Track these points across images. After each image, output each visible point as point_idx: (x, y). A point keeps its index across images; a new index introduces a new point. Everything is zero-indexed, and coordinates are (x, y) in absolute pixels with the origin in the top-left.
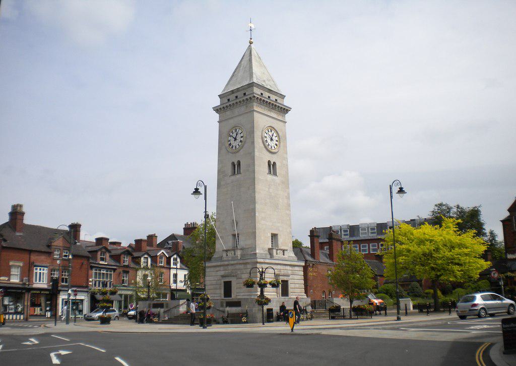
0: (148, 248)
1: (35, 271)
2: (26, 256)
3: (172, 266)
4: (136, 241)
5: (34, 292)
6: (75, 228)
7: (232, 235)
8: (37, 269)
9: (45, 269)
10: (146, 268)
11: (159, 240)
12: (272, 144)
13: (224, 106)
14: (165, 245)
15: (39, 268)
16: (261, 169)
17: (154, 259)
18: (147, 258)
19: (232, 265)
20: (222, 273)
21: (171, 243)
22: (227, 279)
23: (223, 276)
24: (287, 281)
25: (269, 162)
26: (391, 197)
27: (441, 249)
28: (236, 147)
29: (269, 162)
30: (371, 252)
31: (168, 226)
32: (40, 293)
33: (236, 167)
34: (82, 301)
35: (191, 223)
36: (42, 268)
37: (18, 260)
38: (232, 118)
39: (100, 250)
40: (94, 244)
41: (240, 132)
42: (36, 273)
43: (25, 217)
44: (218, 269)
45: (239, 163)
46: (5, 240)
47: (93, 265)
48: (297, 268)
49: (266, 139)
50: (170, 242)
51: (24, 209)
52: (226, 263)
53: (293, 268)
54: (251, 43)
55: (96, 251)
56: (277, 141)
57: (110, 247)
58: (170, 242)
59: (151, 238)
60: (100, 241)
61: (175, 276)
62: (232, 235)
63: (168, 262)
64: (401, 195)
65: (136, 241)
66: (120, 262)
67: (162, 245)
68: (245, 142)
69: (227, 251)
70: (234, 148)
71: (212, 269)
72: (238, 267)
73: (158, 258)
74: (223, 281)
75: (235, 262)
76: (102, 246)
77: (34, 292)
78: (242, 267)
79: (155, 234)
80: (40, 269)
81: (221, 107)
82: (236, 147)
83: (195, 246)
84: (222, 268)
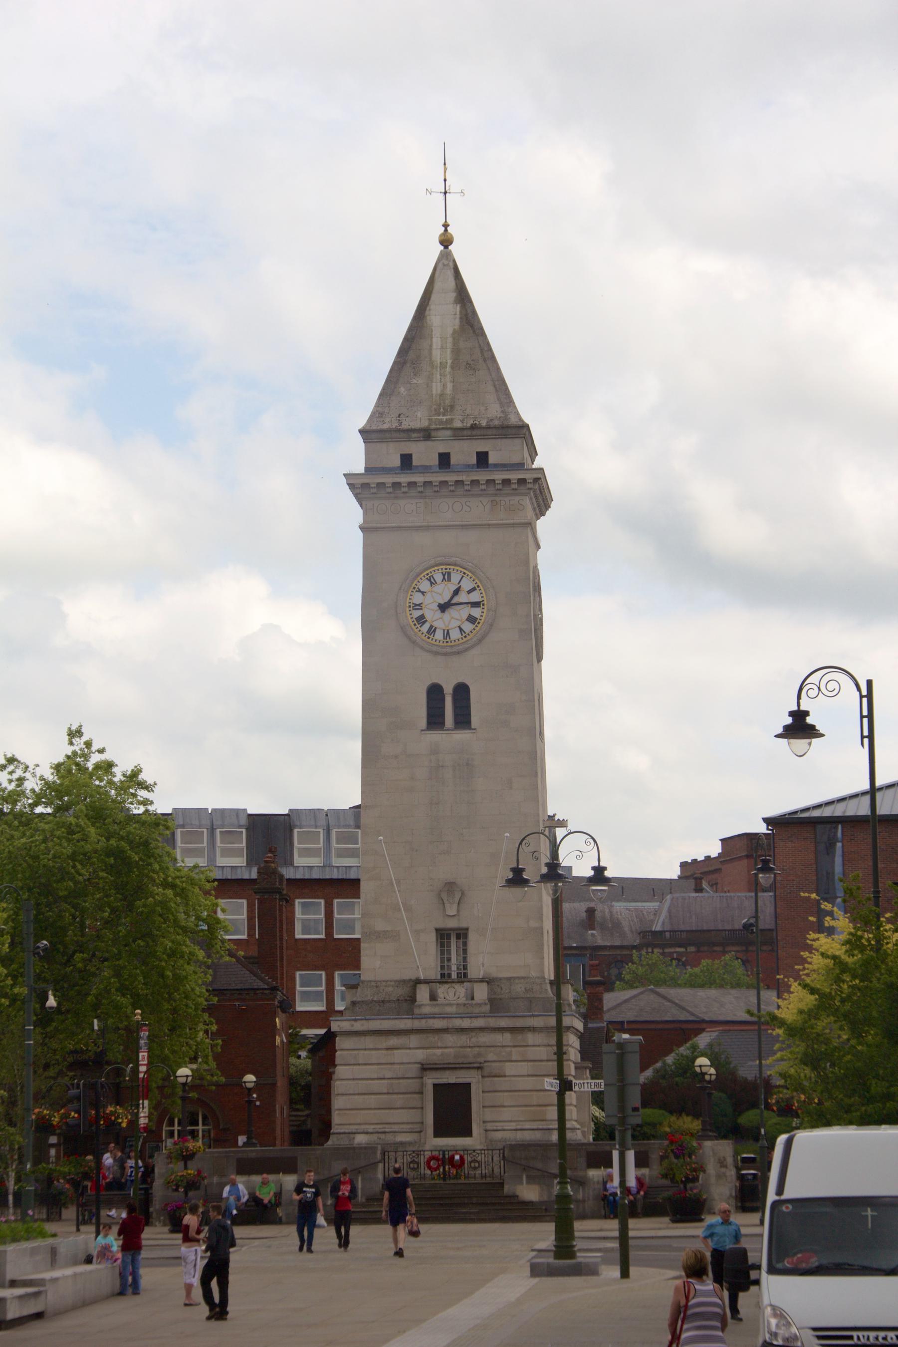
7: (437, 930)
19: (462, 1030)
20: (421, 1055)
23: (426, 1068)
27: (115, 809)
30: (299, 936)
33: (449, 707)
38: (428, 528)
41: (467, 585)
44: (393, 1041)
48: (531, 1038)
53: (520, 1037)
62: (437, 930)
64: (800, 744)
70: (439, 635)
74: (430, 1080)
82: (447, 634)
84: (414, 1040)
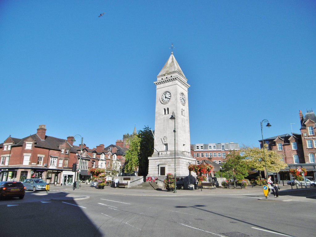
1: (51, 160)
5: (50, 171)
8: (52, 159)
9: (56, 159)
11: (105, 147)
15: (53, 158)
26: (262, 128)
32: (53, 172)
34: (41, 158)
36: (55, 158)
42: (51, 161)
43: (47, 132)
44: (156, 160)
45: (168, 109)
50: (110, 148)
52: (161, 158)
58: (110, 148)
72: (168, 160)
75: (167, 157)
77: (50, 171)
78: (206, 161)
80: (54, 159)
82: (164, 101)
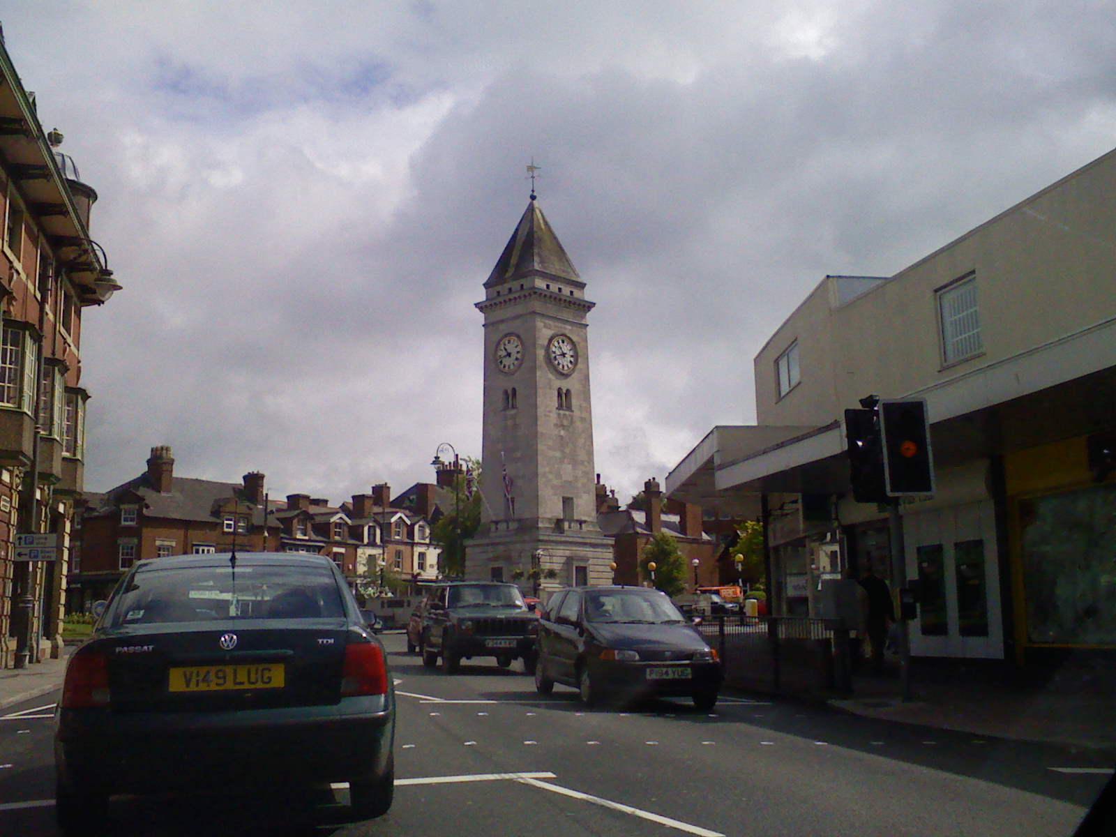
0: (377, 509)
2: (180, 533)
3: (417, 540)
4: (354, 497)
6: (254, 481)
10: (372, 544)
12: (566, 362)
13: (493, 302)
14: (403, 502)
16: (547, 402)
17: (386, 528)
18: (374, 527)
21: (417, 498)
22: (496, 565)
23: (490, 560)
24: (585, 568)
25: (560, 390)
28: (509, 367)
29: (560, 390)
31: (406, 469)
33: (510, 397)
35: (450, 463)
37: (168, 537)
39: (297, 515)
40: (285, 507)
45: (514, 390)
46: (147, 507)
47: (286, 541)
49: (554, 355)
51: (173, 454)
54: (533, 198)
55: (290, 520)
56: (572, 356)
57: (313, 510)
59: (380, 491)
60: (294, 500)
61: (422, 555)
63: (411, 534)
65: (354, 497)
66: (329, 538)
67: (399, 503)
68: (522, 360)
69: (496, 523)
70: (507, 368)
71: (477, 550)
73: (393, 526)
76: (296, 512)
79: (386, 484)
81: (488, 304)
82: (509, 367)
83: (450, 507)
